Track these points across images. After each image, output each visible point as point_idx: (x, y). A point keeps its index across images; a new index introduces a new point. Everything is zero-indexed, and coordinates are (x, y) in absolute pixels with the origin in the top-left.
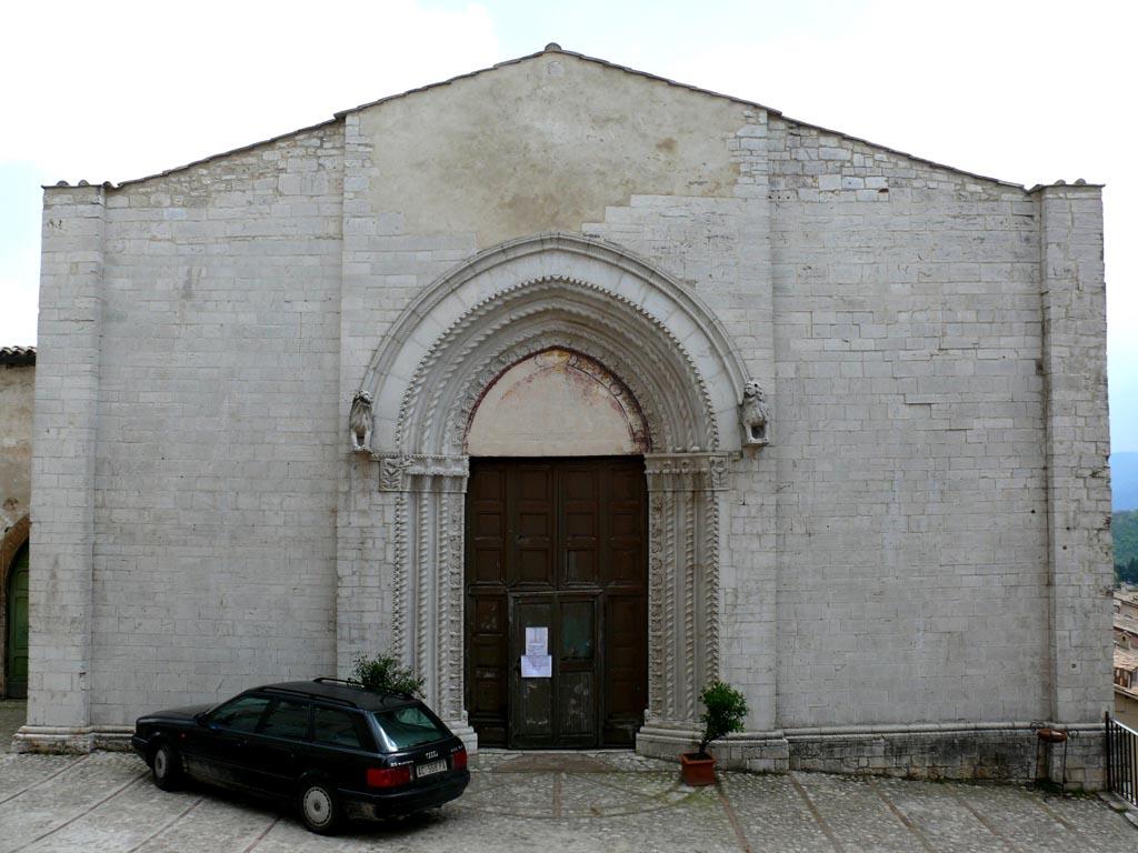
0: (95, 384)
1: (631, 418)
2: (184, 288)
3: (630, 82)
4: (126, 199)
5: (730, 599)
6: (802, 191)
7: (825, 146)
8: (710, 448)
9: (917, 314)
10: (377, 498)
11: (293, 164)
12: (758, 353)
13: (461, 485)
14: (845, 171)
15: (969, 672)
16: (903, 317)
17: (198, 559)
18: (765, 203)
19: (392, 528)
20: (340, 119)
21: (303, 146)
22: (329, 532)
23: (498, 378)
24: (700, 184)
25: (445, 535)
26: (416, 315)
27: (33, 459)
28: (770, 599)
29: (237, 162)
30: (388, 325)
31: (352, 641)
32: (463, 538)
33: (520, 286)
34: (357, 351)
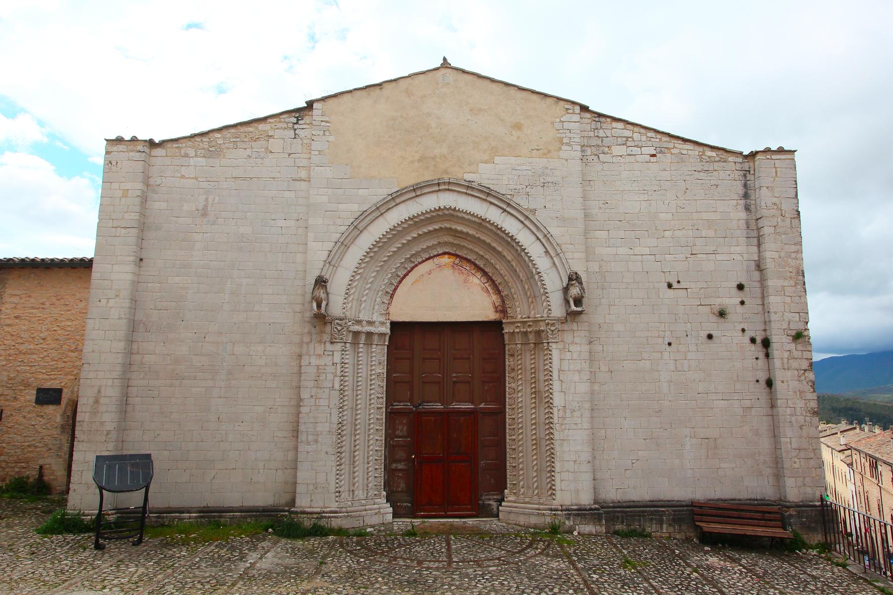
1: (494, 297)
2: (203, 209)
3: (494, 86)
4: (164, 151)
5: (561, 413)
7: (616, 128)
10: (329, 347)
11: (278, 133)
12: (576, 255)
13: (385, 340)
14: (629, 144)
15: (722, 465)
16: (667, 234)
17: (204, 389)
18: (579, 162)
19: (339, 366)
20: (310, 105)
22: (296, 370)
23: (409, 272)
24: (538, 150)
25: (374, 372)
26: (357, 227)
27: (88, 321)
28: (587, 414)
29: (242, 131)
31: (308, 443)
32: (385, 374)
34: (318, 252)
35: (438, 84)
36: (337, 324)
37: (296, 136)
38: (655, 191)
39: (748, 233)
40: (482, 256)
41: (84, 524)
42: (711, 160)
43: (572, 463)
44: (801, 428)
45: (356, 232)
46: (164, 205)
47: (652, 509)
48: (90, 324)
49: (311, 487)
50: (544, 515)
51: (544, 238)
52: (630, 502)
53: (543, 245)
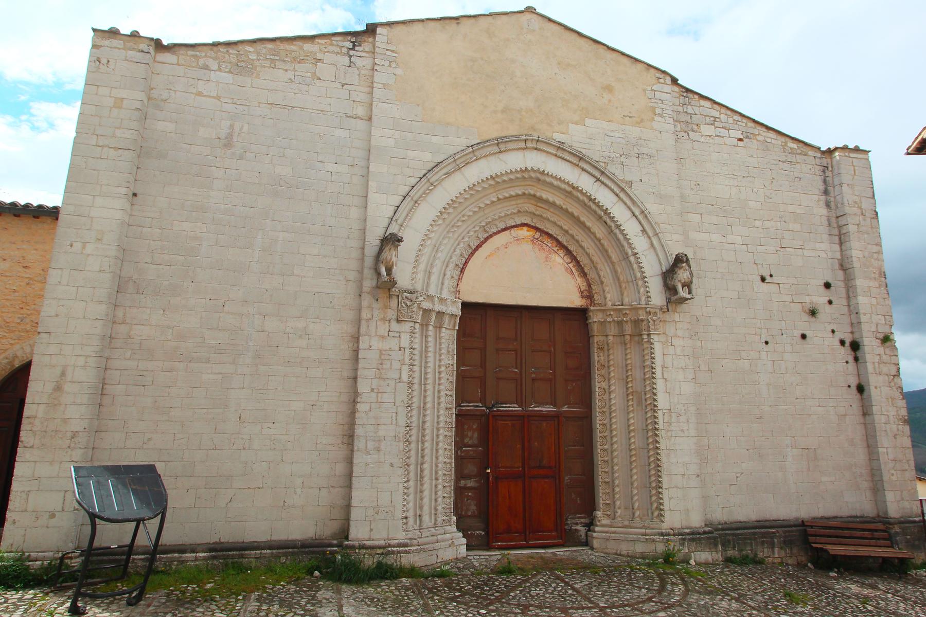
0: (128, 206)
1: (580, 280)
2: (226, 138)
3: (582, 41)
5: (666, 419)
6: (690, 133)
7: (704, 106)
8: (643, 302)
9: (766, 222)
10: (395, 326)
11: (328, 58)
12: (675, 237)
14: (717, 124)
15: (824, 479)
16: (758, 223)
17: (221, 376)
19: (407, 351)
20: (371, 29)
21: (338, 45)
24: (630, 117)
29: (282, 47)
31: (368, 452)
33: (509, 171)
35: (522, 29)
36: (406, 298)
37: (352, 64)
38: (744, 177)
39: (830, 231)
40: (567, 232)
41: (31, 574)
42: (792, 152)
43: (680, 477)
44: (895, 436)
45: (496, 149)
46: (171, 127)
47: (763, 530)
48: (54, 276)
49: (370, 512)
50: (653, 541)
51: (641, 215)
52: (737, 522)
53: (640, 223)
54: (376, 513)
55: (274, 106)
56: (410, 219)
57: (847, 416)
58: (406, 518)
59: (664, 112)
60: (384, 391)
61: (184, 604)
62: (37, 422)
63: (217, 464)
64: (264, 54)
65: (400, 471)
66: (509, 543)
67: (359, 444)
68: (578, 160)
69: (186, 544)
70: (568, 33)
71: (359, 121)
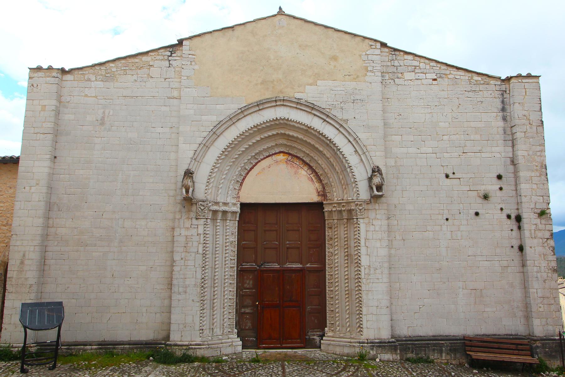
1: (317, 185)
2: (101, 120)
3: (317, 28)
6: (396, 80)
7: (407, 60)
8: (355, 198)
10: (195, 222)
11: (157, 63)
12: (378, 154)
14: (417, 71)
15: (487, 309)
16: (445, 138)
17: (102, 254)
18: (380, 84)
19: (202, 236)
20: (181, 42)
21: (162, 55)
22: (170, 239)
23: (254, 166)
24: (349, 75)
25: (228, 241)
27: (16, 203)
28: (386, 271)
29: (130, 61)
30: (202, 139)
31: (179, 293)
32: (236, 242)
36: (201, 205)
37: (170, 65)
38: (436, 106)
39: (505, 137)
40: (308, 154)
42: (477, 83)
43: (375, 308)
44: (544, 281)
46: (72, 117)
48: (17, 205)
49: (181, 326)
50: (354, 346)
51: (354, 141)
52: (418, 336)
53: (353, 146)
54: (184, 327)
55: (127, 97)
56: (204, 157)
57: (509, 267)
58: (203, 330)
59: (374, 69)
60: (188, 259)
61: (74, 370)
62: (13, 280)
63: (102, 300)
64: (120, 67)
65: (198, 304)
66: (267, 346)
67: (175, 289)
68: (311, 109)
69: (88, 341)
70: (307, 25)
71: (175, 100)
